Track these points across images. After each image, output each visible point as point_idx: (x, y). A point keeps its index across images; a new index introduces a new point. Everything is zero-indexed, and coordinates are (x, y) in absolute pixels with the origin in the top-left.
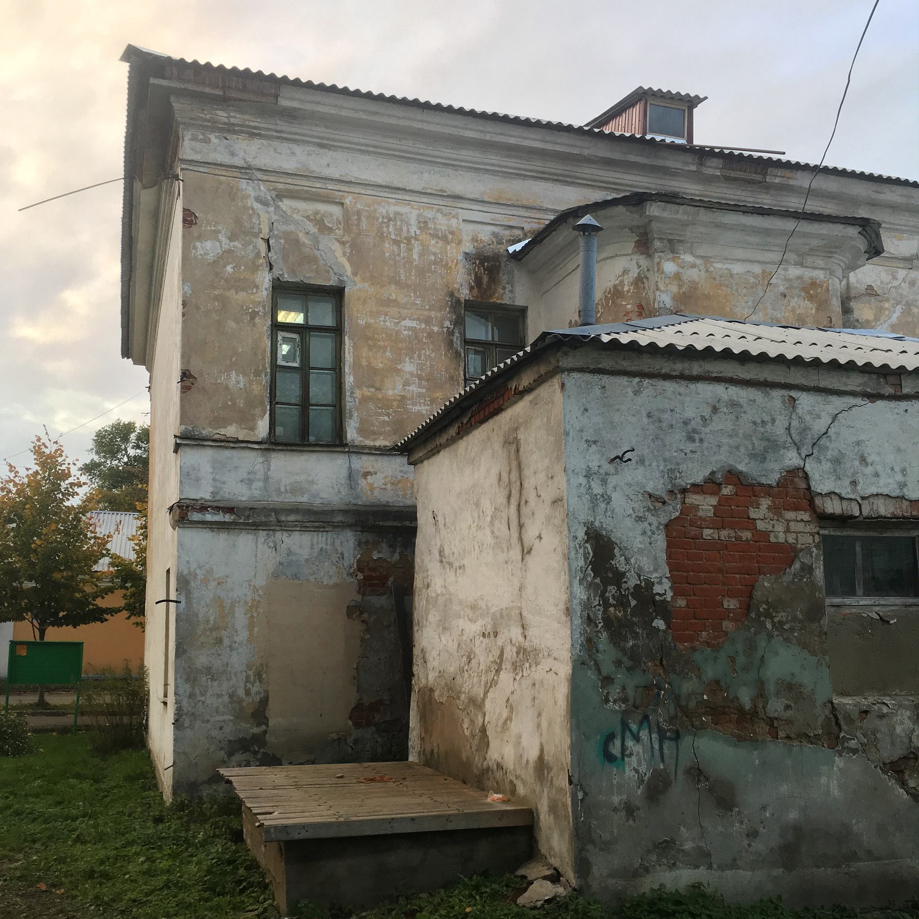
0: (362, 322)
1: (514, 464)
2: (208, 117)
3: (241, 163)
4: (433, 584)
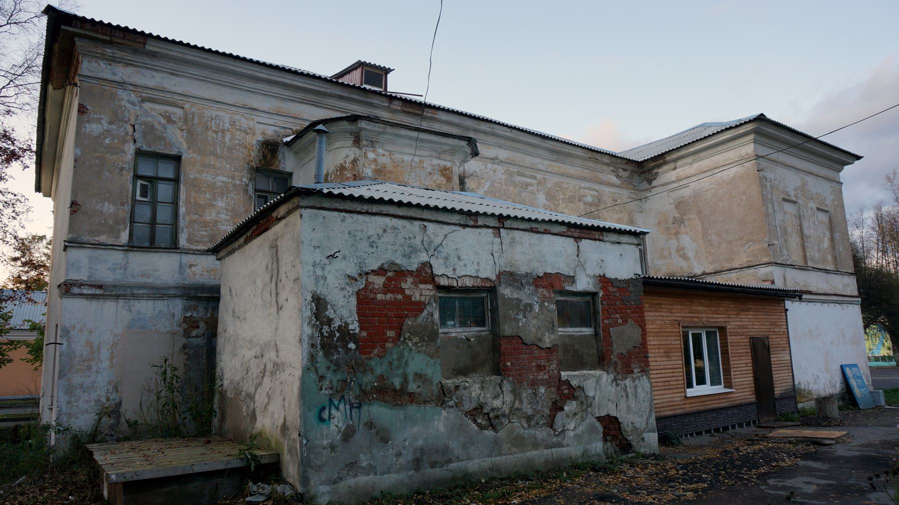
0: (192, 176)
1: (275, 259)
2: (99, 51)
3: (119, 80)
4: (228, 330)
